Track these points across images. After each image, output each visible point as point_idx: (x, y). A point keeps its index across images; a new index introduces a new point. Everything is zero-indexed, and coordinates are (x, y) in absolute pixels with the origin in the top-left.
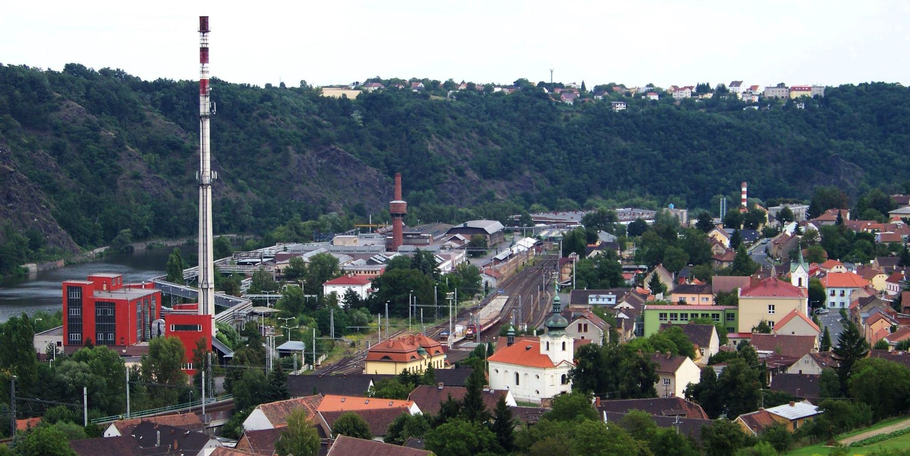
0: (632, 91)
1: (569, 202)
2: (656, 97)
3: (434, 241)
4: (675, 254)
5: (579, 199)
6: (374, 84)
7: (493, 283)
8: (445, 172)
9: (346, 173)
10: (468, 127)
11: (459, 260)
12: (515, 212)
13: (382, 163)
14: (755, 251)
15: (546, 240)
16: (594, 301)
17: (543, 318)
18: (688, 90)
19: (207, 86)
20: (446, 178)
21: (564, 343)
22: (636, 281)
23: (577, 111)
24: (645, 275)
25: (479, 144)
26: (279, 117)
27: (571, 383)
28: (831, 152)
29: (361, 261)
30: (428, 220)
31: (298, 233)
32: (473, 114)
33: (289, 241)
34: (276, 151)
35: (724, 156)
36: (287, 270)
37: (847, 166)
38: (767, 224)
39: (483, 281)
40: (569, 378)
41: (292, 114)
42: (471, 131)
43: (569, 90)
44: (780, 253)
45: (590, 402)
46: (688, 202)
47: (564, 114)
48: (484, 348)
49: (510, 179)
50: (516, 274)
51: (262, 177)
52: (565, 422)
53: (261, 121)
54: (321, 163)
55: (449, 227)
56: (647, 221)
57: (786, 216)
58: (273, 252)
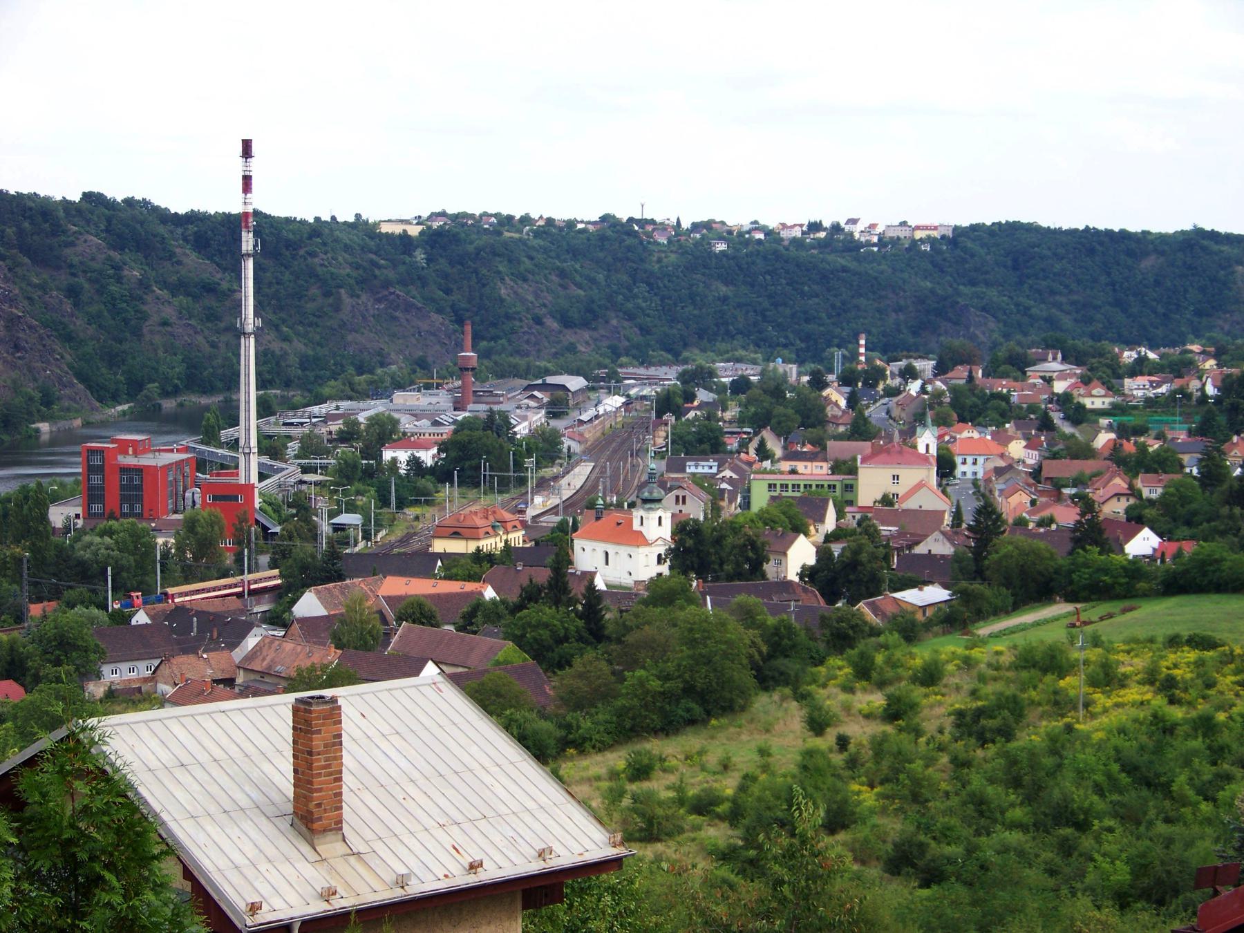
3: (508, 399)
4: (785, 415)
5: (674, 353)
7: (576, 448)
8: (521, 320)
9: (407, 320)
11: (537, 421)
12: (601, 366)
13: (448, 310)
14: (875, 412)
15: (636, 399)
16: (693, 470)
18: (798, 228)
19: (251, 220)
21: (660, 518)
22: (740, 446)
23: (672, 252)
24: (751, 440)
26: (329, 255)
27: (668, 563)
28: (960, 300)
32: (553, 254)
33: (341, 399)
34: (327, 294)
35: (839, 304)
36: (340, 432)
37: (977, 316)
38: (888, 382)
39: (565, 446)
40: (666, 557)
41: (345, 252)
43: (662, 227)
44: (903, 415)
45: (691, 586)
47: (656, 255)
48: (567, 522)
49: (595, 329)
51: (310, 325)
55: (526, 383)
56: (752, 378)
57: (909, 374)
58: (324, 411)
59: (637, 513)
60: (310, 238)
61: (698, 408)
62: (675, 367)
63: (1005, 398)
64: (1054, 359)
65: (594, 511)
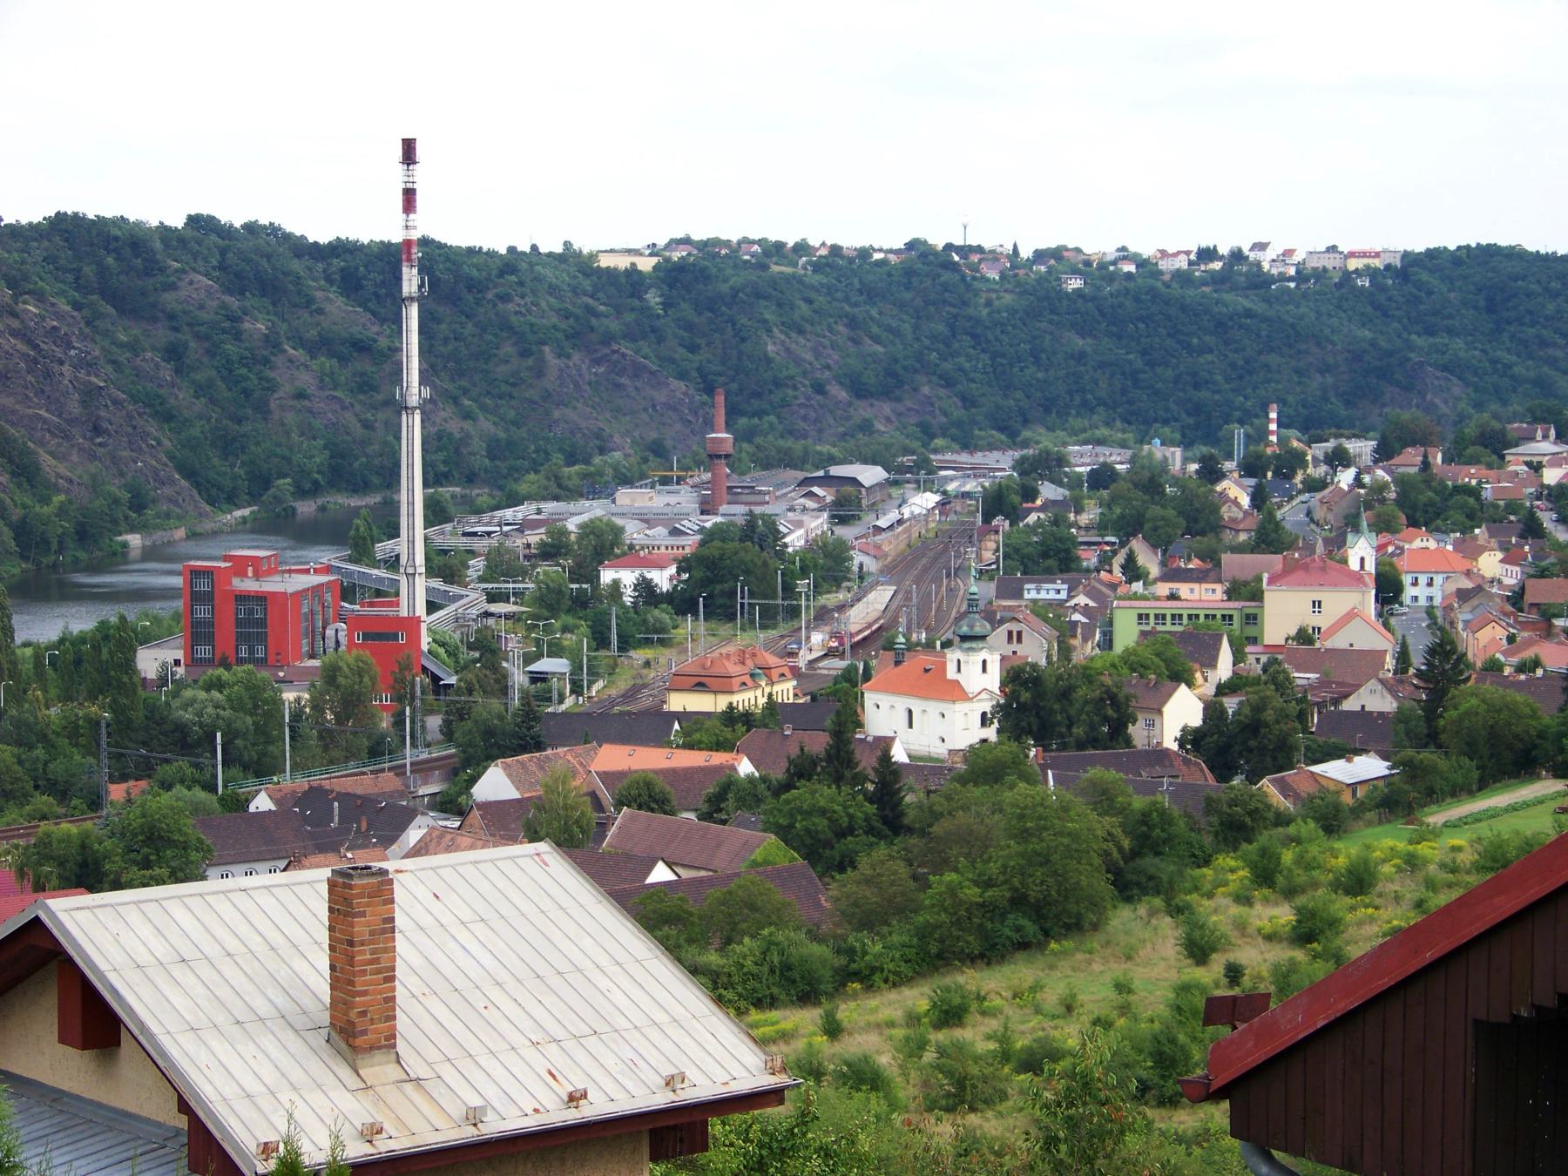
0: (1093, 258)
1: (992, 436)
2: (1132, 268)
4: (1163, 518)
5: (1009, 430)
6: (681, 246)
7: (871, 565)
8: (795, 388)
9: (637, 389)
10: (831, 316)
11: (817, 528)
12: (907, 451)
13: (694, 374)
14: (1290, 513)
15: (956, 497)
16: (1033, 595)
17: (951, 620)
18: (1183, 257)
19: (414, 250)
20: (796, 397)
21: (984, 662)
23: (1006, 291)
25: (849, 343)
26: (528, 300)
27: (996, 725)
28: (1412, 355)
29: (660, 531)
30: (767, 465)
31: (560, 486)
33: (544, 499)
34: (524, 354)
35: (1241, 363)
37: (1438, 378)
39: (856, 562)
41: (551, 294)
42: (836, 323)
43: (993, 256)
44: (1330, 517)
46: (1183, 435)
47: (984, 295)
48: (857, 669)
49: (898, 400)
50: (908, 551)
52: (987, 788)
53: (500, 306)
54: (596, 374)
55: (801, 475)
56: (1118, 467)
57: (1339, 459)
58: (520, 516)
59: (952, 656)
60: (501, 274)
61: (1041, 509)
62: (1011, 453)
63: (1474, 492)
64: (1545, 437)
65: (892, 653)
